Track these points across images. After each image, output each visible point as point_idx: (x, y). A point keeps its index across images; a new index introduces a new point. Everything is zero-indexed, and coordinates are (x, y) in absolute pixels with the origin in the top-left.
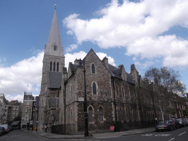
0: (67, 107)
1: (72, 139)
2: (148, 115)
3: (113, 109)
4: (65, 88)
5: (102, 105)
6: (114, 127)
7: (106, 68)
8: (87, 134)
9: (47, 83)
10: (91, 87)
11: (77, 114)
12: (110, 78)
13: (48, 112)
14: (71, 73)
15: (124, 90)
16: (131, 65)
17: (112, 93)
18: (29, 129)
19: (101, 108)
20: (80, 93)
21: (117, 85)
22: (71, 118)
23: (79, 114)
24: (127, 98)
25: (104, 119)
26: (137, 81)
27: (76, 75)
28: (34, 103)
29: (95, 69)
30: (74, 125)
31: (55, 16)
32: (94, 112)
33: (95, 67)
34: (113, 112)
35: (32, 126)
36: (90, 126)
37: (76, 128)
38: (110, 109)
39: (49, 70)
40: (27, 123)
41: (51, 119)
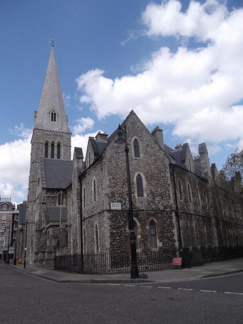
0: (87, 221)
1: (105, 283)
2: (229, 237)
3: (175, 225)
4: (81, 186)
6: (180, 259)
8: (135, 274)
9: (40, 180)
12: (168, 166)
13: (44, 231)
14: (92, 156)
17: (171, 195)
18: (8, 262)
19: (152, 223)
20: (113, 194)
21: (179, 181)
22: (95, 243)
23: (112, 233)
24: (195, 204)
25: (160, 244)
26: (210, 174)
27: (104, 160)
28: (15, 217)
29: (141, 149)
30: (102, 255)
31: (51, 60)
32: (139, 230)
33: (140, 145)
34: (175, 231)
35: (11, 256)
37: (108, 262)
39: (44, 156)
40: (4, 252)
41: (51, 243)
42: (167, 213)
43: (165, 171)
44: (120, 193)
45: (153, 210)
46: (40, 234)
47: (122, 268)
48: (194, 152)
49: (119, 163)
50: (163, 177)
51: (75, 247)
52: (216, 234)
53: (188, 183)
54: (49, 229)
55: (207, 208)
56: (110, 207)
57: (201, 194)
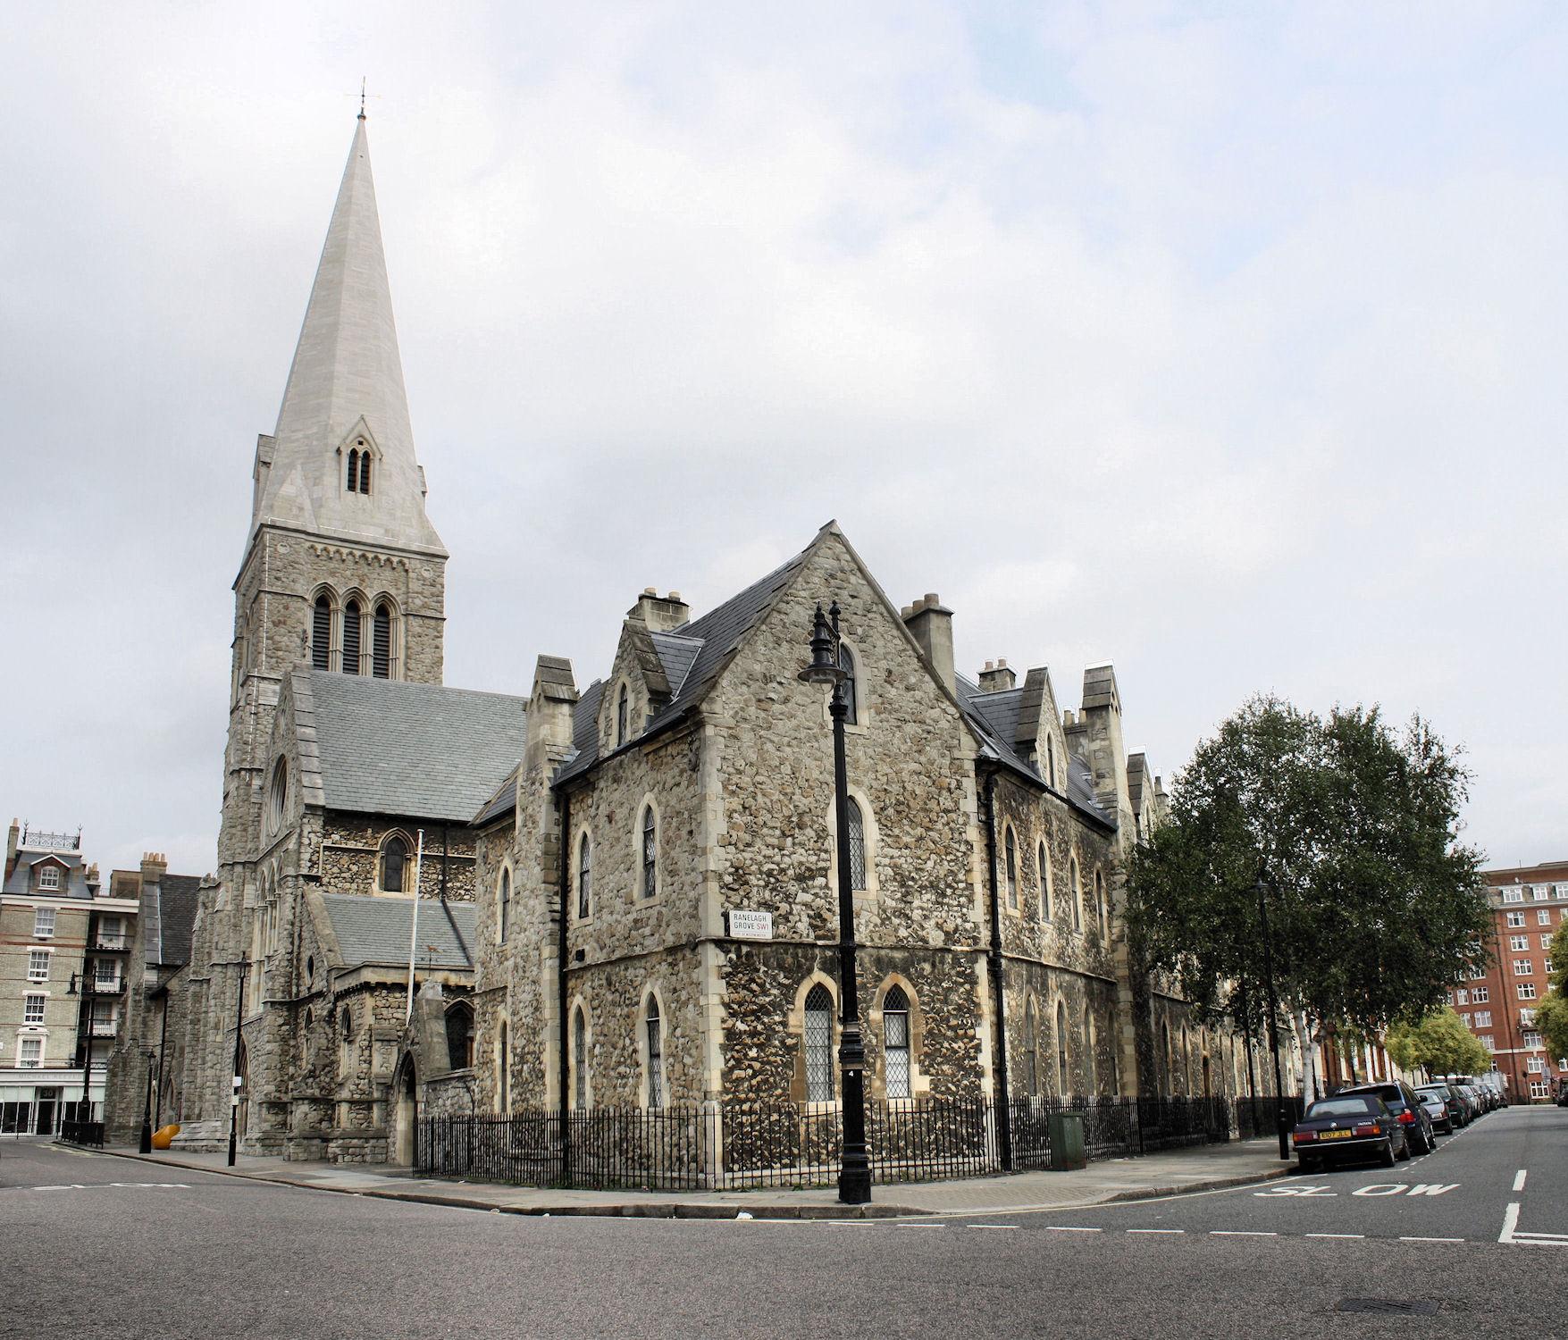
1: (799, 1217)
4: (566, 824)
5: (911, 980)
7: (941, 687)
10: (822, 835)
11: (717, 1037)
12: (969, 766)
13: (320, 1009)
15: (1048, 865)
16: (1088, 672)
22: (644, 1069)
23: (730, 1034)
25: (922, 1084)
27: (709, 731)
34: (984, 1033)
36: (813, 1128)
37: (716, 1144)
38: (959, 1008)
40: (42, 1091)
42: (956, 962)
43: (959, 787)
44: (770, 874)
45: (903, 948)
46: (292, 1021)
47: (767, 1172)
48: (1068, 698)
49: (769, 746)
50: (946, 811)
51: (527, 1081)
52: (1130, 1050)
53: (1039, 838)
54: (352, 1001)
55: (1104, 944)
56: (727, 929)
57: (1085, 885)
